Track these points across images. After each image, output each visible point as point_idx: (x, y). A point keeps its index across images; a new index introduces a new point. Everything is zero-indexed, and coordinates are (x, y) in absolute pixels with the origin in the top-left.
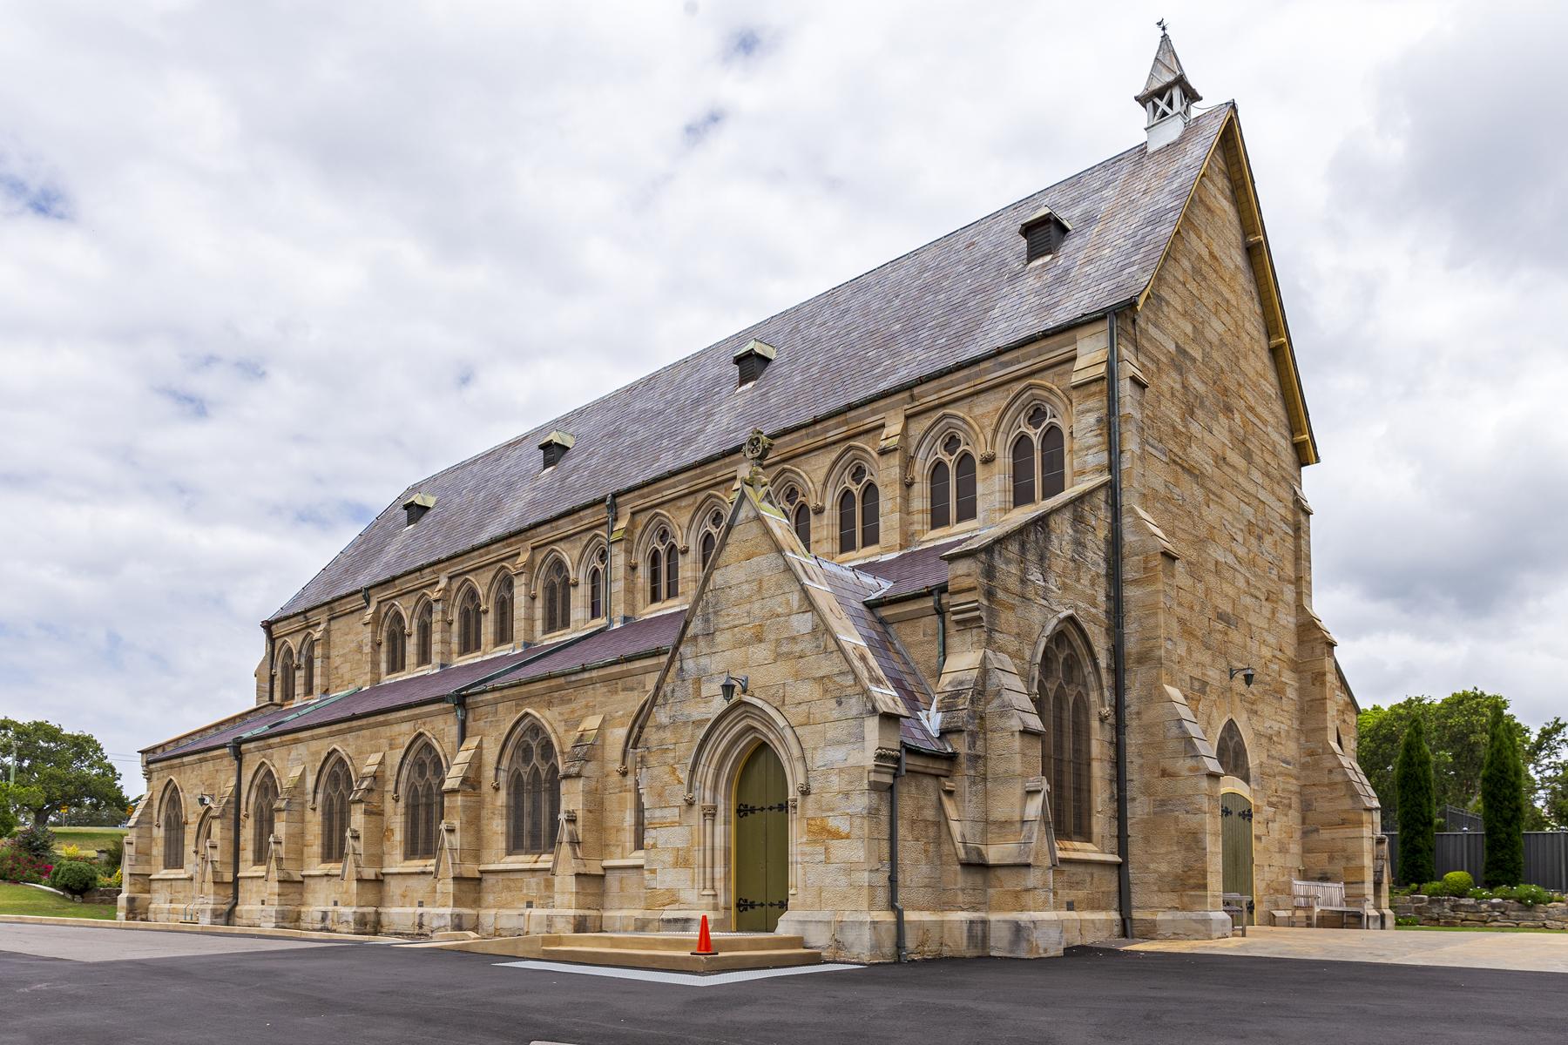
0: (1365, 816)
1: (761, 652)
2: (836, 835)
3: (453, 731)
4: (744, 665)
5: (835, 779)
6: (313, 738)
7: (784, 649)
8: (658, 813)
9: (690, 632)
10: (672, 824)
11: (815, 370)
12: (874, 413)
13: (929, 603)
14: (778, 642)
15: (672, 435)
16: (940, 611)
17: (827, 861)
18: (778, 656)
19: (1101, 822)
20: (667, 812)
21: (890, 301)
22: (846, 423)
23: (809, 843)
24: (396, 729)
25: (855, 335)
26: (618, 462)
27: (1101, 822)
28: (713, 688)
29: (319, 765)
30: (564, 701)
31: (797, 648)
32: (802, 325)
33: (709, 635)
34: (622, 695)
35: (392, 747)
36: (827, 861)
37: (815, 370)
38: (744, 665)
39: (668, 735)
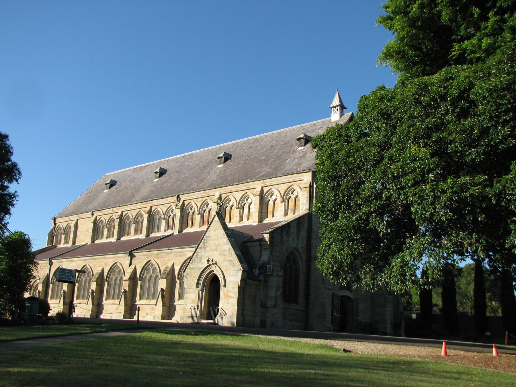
0: (388, 304)
1: (217, 253)
2: (231, 297)
3: (128, 262)
4: (212, 256)
5: (231, 284)
6: (78, 260)
7: (222, 253)
8: (188, 290)
9: (200, 246)
10: (192, 293)
11: (240, 166)
12: (254, 184)
13: (258, 243)
14: (221, 251)
15: (197, 177)
16: (260, 245)
17: (228, 303)
18: (220, 254)
19: (301, 299)
20: (191, 290)
21: (263, 148)
22: (246, 186)
23: (224, 299)
24: (108, 260)
25: (252, 156)
26: (180, 182)
27: (301, 299)
28: (205, 260)
29: (196, 281)
30: (162, 257)
31: (225, 253)
32: (238, 148)
33: (205, 247)
34: (179, 258)
35: (106, 265)
36: (228, 303)
37: (240, 166)
38: (212, 256)
39: (193, 271)
